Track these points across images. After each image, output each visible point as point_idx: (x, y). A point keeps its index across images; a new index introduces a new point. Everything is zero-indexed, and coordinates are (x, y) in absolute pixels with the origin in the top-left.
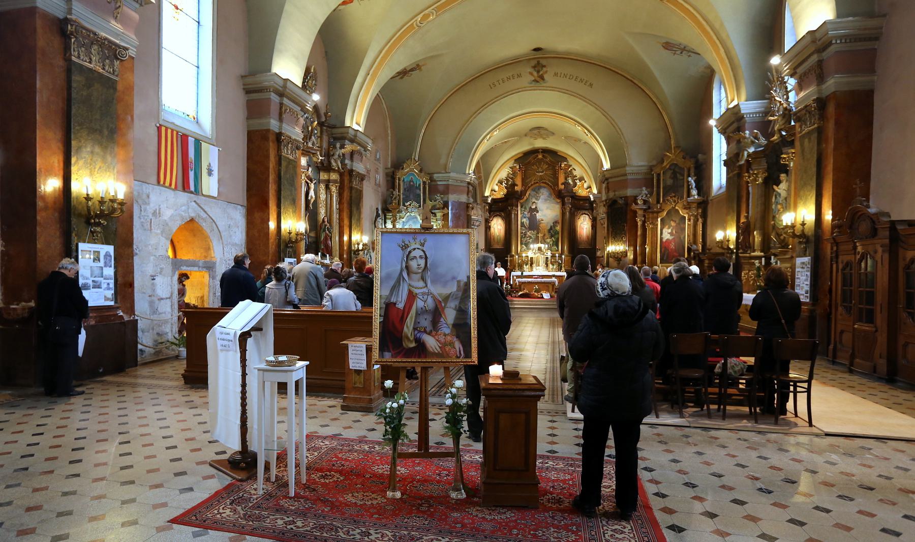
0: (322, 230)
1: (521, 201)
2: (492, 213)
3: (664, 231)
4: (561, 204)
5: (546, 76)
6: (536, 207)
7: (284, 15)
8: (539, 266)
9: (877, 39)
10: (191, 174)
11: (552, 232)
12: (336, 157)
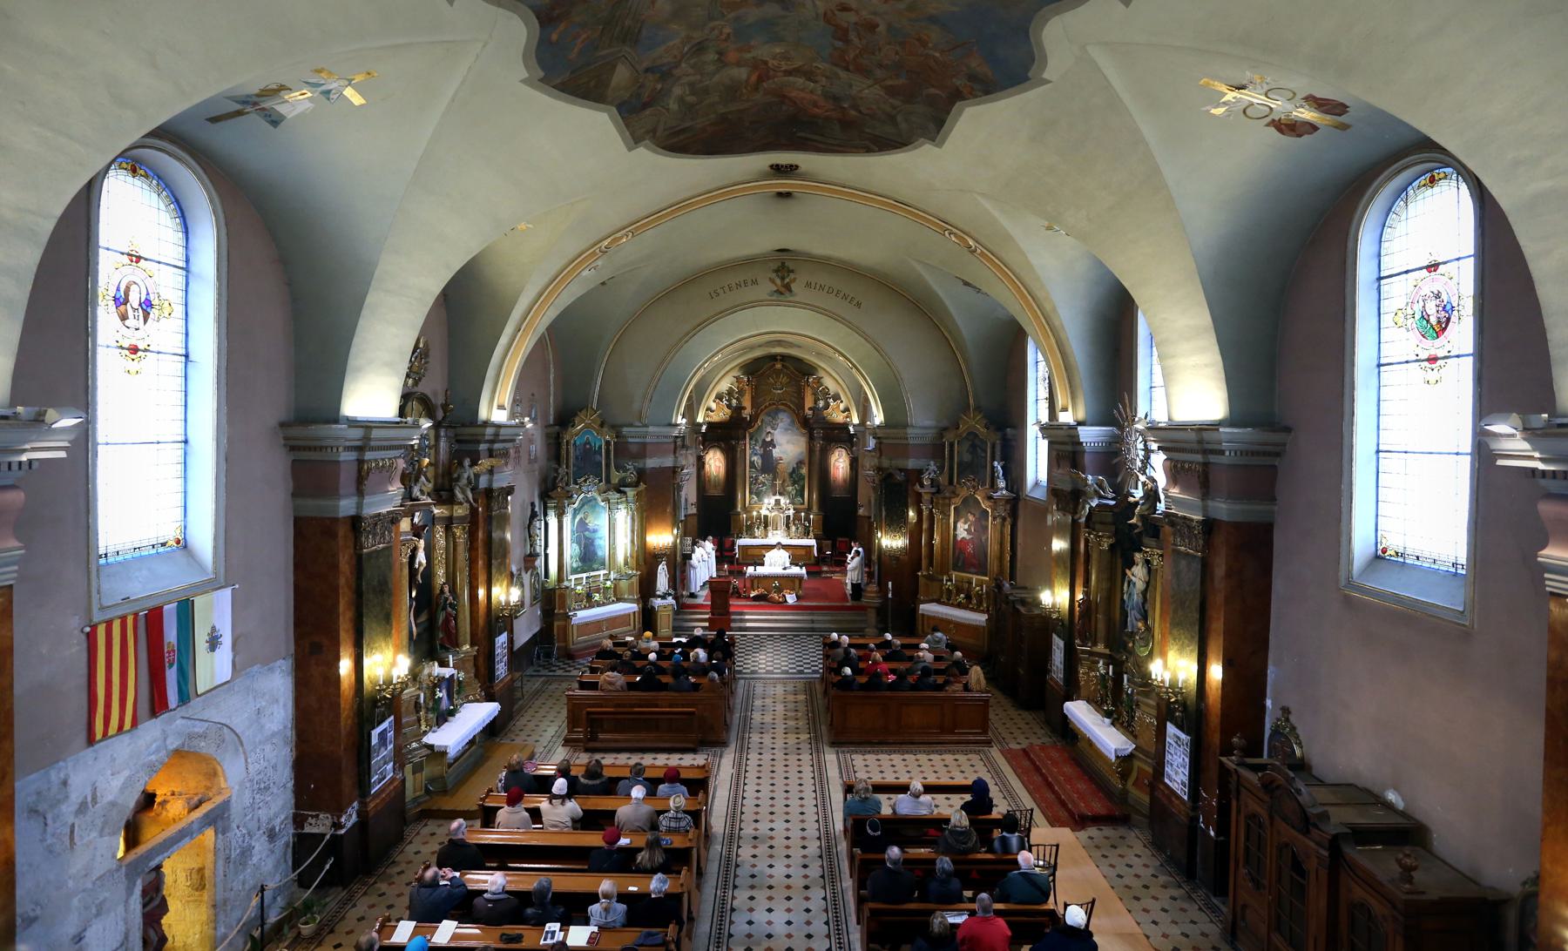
0: (440, 608)
1: (751, 430)
2: (707, 443)
3: (959, 525)
4: (807, 435)
5: (793, 286)
6: (772, 440)
7: (365, 312)
8: (776, 529)
9: (1278, 455)
10: (171, 675)
11: (795, 476)
12: (464, 481)
